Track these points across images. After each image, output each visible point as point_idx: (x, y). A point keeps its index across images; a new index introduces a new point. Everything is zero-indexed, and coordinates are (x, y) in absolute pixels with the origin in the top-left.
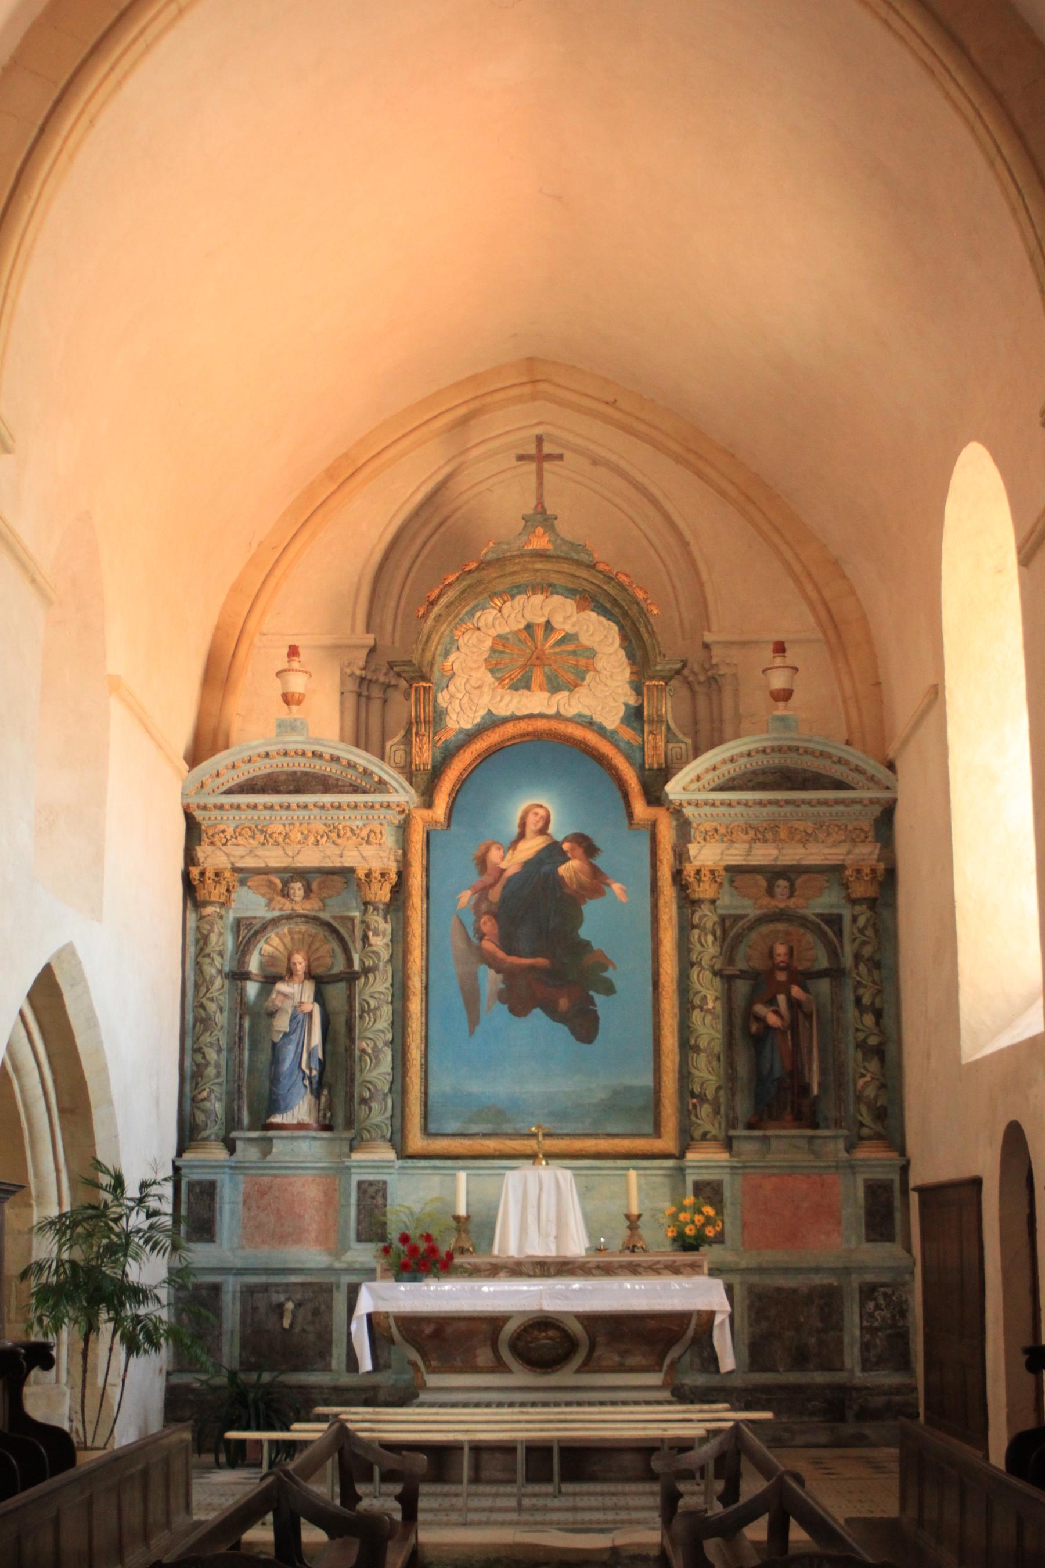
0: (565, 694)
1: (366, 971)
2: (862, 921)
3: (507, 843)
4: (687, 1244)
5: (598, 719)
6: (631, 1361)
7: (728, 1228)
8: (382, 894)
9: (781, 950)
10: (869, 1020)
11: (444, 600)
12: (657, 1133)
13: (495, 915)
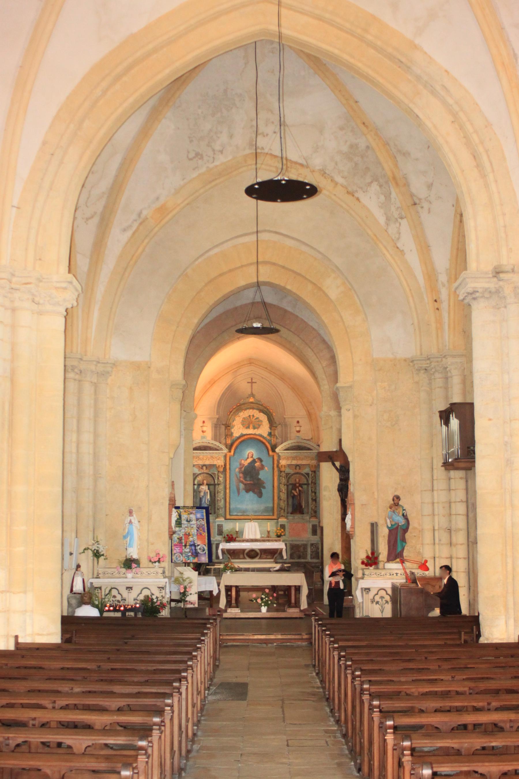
0: (256, 429)
1: (218, 484)
2: (313, 475)
3: (245, 459)
4: (279, 536)
5: (263, 434)
6: (268, 557)
7: (286, 534)
8: (221, 469)
9: (297, 480)
10: (313, 494)
11: (233, 412)
12: (273, 515)
13: (243, 473)
